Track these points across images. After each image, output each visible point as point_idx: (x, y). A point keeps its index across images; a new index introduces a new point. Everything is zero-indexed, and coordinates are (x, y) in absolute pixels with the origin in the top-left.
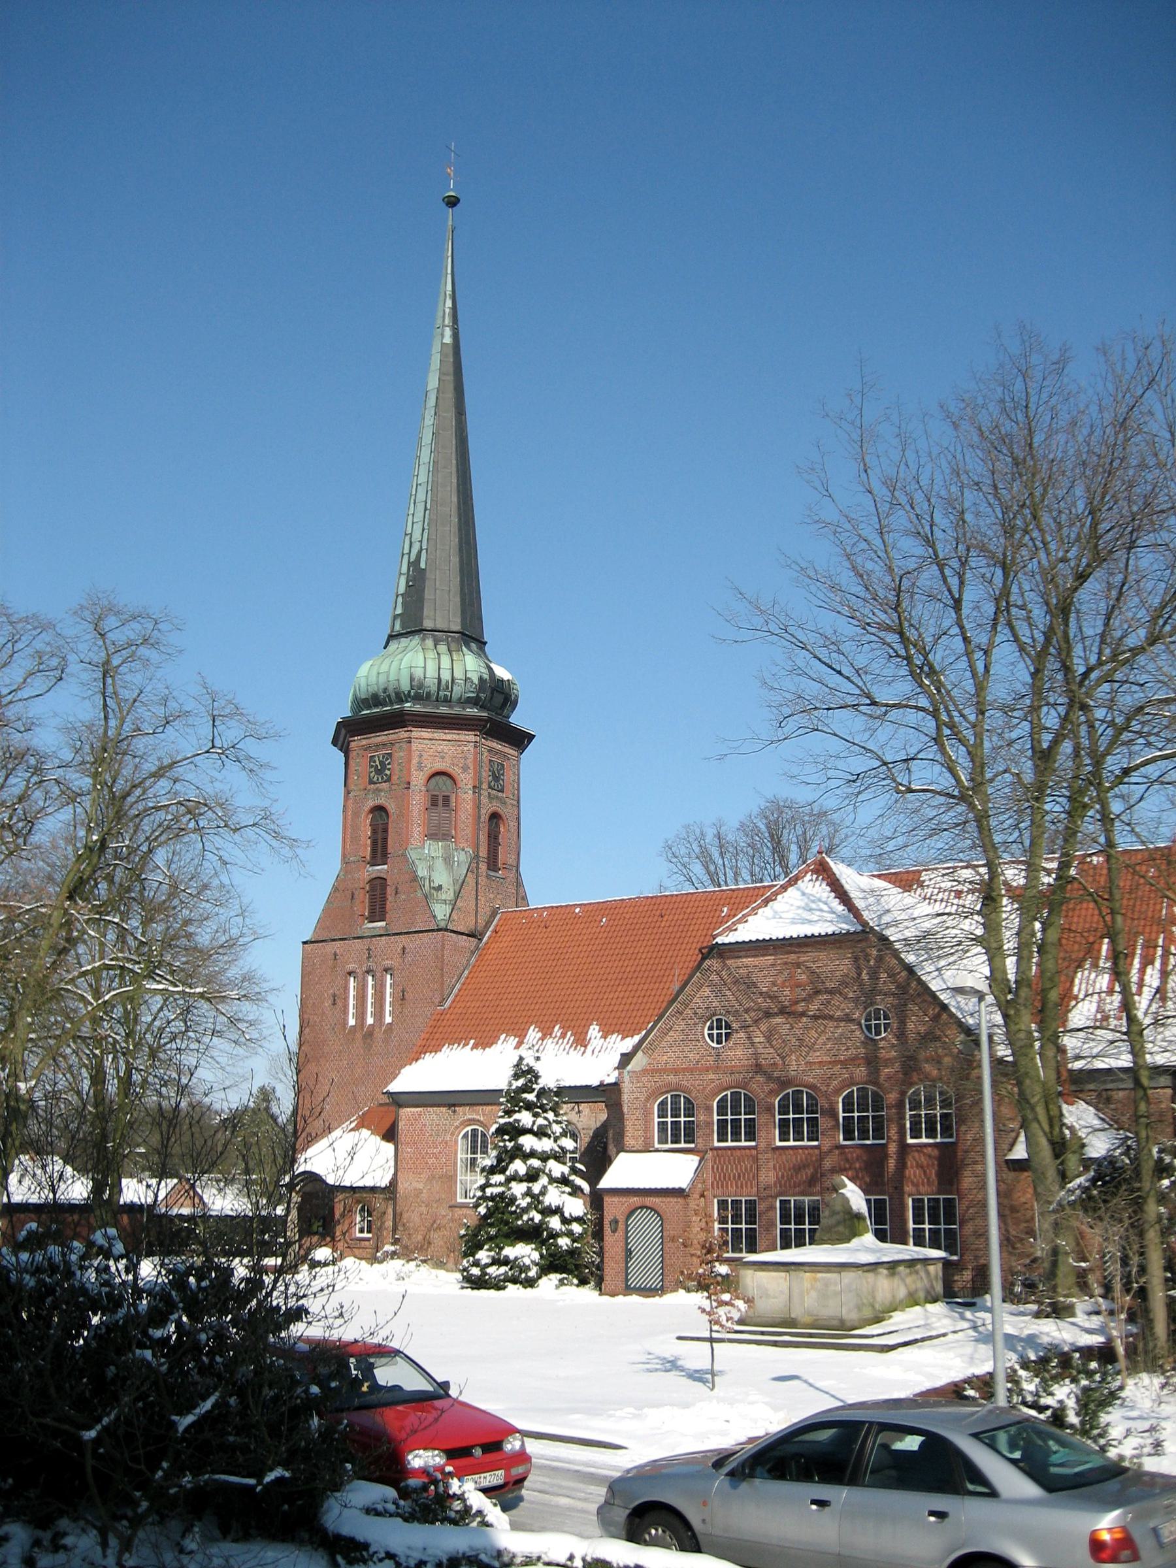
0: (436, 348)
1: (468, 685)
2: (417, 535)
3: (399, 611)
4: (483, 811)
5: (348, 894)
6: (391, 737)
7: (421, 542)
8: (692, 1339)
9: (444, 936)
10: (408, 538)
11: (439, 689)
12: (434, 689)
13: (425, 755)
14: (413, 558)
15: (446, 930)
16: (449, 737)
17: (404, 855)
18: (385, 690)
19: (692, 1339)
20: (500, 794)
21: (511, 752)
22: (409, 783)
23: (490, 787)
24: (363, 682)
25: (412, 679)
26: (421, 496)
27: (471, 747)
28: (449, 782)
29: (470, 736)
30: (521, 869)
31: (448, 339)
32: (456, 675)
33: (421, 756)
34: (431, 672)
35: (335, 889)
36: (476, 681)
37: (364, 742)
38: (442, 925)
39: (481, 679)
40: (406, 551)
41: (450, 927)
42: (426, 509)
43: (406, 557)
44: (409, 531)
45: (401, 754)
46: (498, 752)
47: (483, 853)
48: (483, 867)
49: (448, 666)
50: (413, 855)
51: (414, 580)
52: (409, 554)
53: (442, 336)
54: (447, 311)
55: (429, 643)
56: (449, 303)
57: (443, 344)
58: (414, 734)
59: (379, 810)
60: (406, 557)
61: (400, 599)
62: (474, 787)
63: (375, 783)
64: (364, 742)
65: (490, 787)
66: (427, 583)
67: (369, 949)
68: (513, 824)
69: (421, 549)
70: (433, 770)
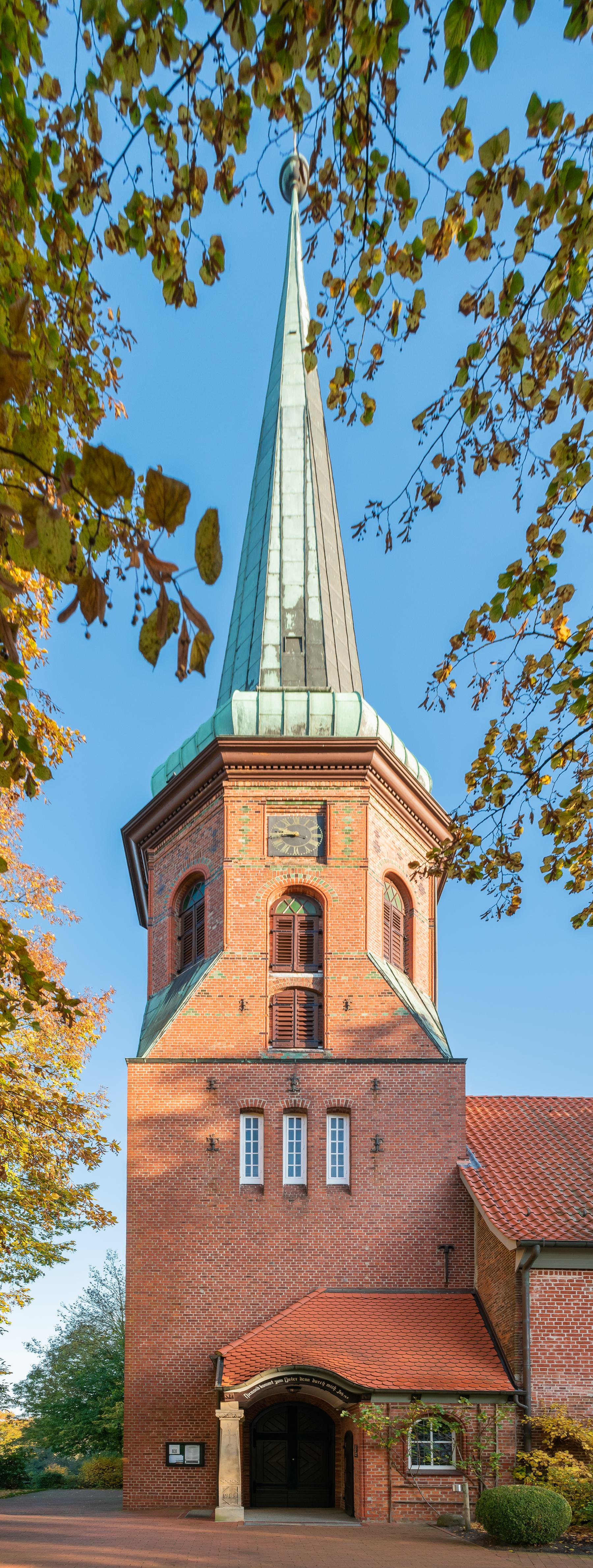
37: (262, 792)
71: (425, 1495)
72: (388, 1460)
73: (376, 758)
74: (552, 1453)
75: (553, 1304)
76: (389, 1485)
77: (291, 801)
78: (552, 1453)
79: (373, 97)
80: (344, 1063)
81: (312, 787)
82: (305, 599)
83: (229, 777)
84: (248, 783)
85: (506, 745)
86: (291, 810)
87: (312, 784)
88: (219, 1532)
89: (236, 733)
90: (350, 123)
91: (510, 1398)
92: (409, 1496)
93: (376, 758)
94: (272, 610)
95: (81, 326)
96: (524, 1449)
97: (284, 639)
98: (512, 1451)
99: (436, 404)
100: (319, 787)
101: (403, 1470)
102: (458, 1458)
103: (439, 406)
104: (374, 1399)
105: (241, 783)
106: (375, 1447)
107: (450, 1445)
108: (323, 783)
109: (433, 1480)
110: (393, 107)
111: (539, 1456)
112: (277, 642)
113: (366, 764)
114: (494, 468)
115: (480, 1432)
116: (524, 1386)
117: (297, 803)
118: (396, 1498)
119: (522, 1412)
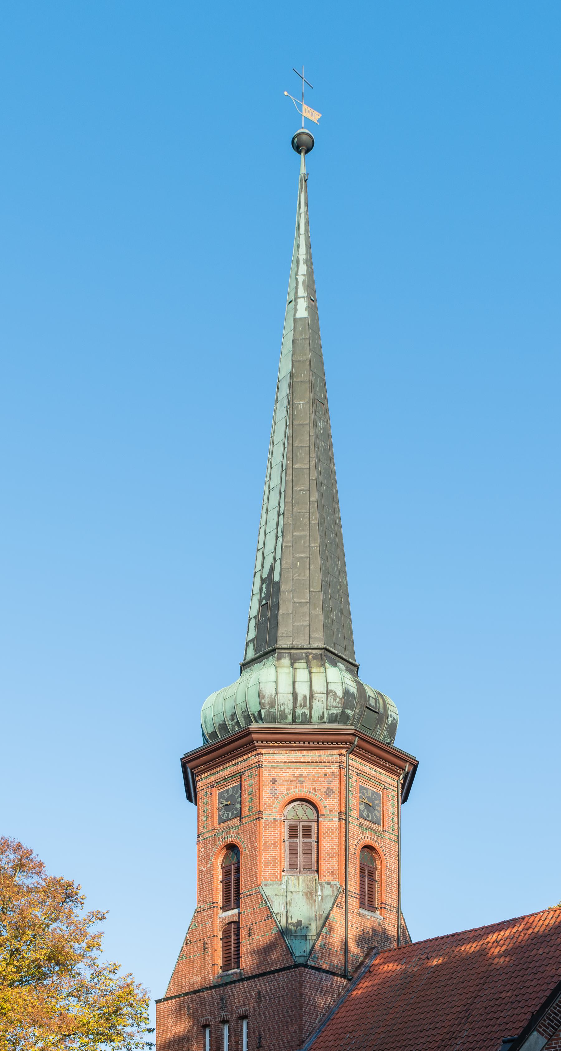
0: (290, 324)
1: (330, 699)
2: (270, 547)
3: (252, 635)
4: (352, 842)
5: (200, 944)
6: (239, 766)
7: (274, 553)
8: (265, 540)
9: (301, 972)
10: (260, 553)
11: (295, 707)
12: (289, 707)
13: (279, 781)
14: (265, 574)
15: (306, 966)
16: (308, 758)
17: (259, 893)
18: (233, 716)
19: (265, 540)
20: (375, 827)
21: (388, 780)
22: (260, 812)
23: (361, 816)
24: (209, 714)
25: (261, 696)
26: (274, 502)
27: (335, 768)
28: (310, 811)
29: (333, 756)
30: (403, 908)
31: (302, 312)
32: (315, 689)
33: (274, 782)
34: (285, 688)
35: (188, 942)
36: (340, 694)
37: (212, 778)
38: (301, 960)
39: (346, 692)
40: (259, 567)
41: (310, 963)
42: (279, 514)
43: (258, 575)
44: (261, 545)
45: (252, 781)
46: (370, 778)
47: (354, 886)
48: (354, 903)
49: (307, 678)
50: (268, 891)
51: (267, 597)
52: (261, 571)
53: (295, 309)
54: (301, 279)
55: (286, 661)
56: (303, 269)
57: (295, 320)
58: (263, 758)
59: (232, 848)
60: (258, 575)
61: (253, 622)
62: (340, 813)
63: (225, 821)
64: (212, 778)
65: (361, 816)
66: (282, 596)
67: (222, 999)
68: (392, 862)
69: (275, 561)
70: (291, 797)
75: (329, 834)
77: (226, 779)
79: (321, 459)
80: (244, 981)
81: (235, 765)
83: (197, 774)
84: (206, 774)
86: (228, 785)
87: (234, 762)
89: (197, 779)
90: (387, 724)
95: (225, 925)
99: (543, 912)
100: (238, 763)
103: (546, 914)
105: (203, 776)
108: (240, 759)
114: (95, 935)
117: (229, 779)
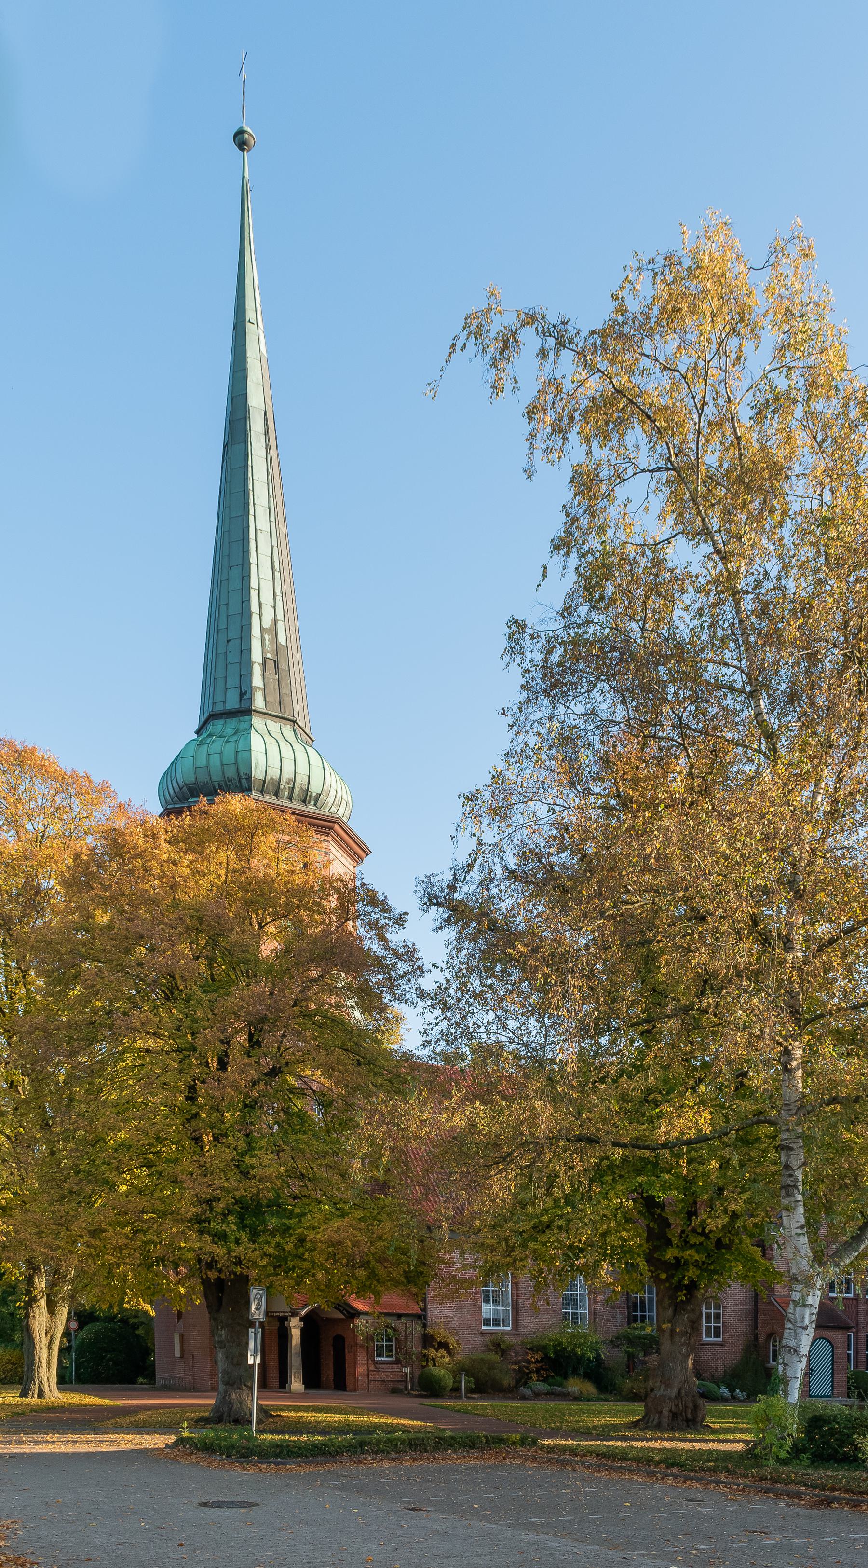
71: (384, 1376)
72: (368, 1354)
73: (336, 827)
74: (437, 1350)
76: (368, 1370)
78: (437, 1350)
82: (275, 620)
85: (554, 1346)
88: (351, 1418)
91: (419, 1317)
92: (377, 1377)
93: (336, 827)
94: (256, 631)
96: (425, 1347)
97: (265, 659)
98: (420, 1349)
101: (373, 1360)
102: (397, 1353)
104: (361, 1316)
106: (362, 1346)
107: (392, 1345)
109: (387, 1366)
110: (575, 1385)
111: (432, 1352)
112: (261, 662)
113: (332, 828)
115: (406, 1338)
116: (424, 1310)
118: (371, 1378)
119: (425, 1326)
